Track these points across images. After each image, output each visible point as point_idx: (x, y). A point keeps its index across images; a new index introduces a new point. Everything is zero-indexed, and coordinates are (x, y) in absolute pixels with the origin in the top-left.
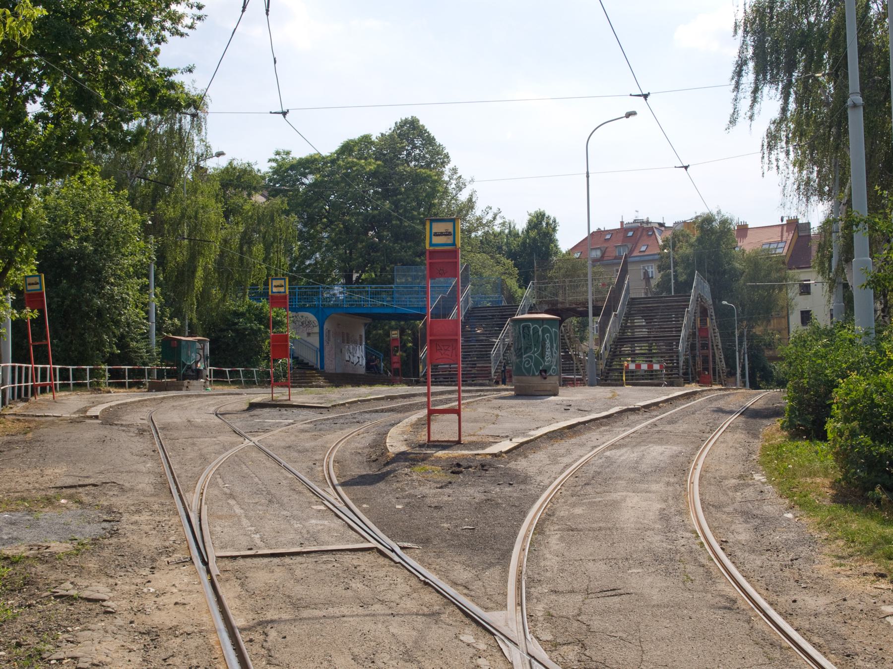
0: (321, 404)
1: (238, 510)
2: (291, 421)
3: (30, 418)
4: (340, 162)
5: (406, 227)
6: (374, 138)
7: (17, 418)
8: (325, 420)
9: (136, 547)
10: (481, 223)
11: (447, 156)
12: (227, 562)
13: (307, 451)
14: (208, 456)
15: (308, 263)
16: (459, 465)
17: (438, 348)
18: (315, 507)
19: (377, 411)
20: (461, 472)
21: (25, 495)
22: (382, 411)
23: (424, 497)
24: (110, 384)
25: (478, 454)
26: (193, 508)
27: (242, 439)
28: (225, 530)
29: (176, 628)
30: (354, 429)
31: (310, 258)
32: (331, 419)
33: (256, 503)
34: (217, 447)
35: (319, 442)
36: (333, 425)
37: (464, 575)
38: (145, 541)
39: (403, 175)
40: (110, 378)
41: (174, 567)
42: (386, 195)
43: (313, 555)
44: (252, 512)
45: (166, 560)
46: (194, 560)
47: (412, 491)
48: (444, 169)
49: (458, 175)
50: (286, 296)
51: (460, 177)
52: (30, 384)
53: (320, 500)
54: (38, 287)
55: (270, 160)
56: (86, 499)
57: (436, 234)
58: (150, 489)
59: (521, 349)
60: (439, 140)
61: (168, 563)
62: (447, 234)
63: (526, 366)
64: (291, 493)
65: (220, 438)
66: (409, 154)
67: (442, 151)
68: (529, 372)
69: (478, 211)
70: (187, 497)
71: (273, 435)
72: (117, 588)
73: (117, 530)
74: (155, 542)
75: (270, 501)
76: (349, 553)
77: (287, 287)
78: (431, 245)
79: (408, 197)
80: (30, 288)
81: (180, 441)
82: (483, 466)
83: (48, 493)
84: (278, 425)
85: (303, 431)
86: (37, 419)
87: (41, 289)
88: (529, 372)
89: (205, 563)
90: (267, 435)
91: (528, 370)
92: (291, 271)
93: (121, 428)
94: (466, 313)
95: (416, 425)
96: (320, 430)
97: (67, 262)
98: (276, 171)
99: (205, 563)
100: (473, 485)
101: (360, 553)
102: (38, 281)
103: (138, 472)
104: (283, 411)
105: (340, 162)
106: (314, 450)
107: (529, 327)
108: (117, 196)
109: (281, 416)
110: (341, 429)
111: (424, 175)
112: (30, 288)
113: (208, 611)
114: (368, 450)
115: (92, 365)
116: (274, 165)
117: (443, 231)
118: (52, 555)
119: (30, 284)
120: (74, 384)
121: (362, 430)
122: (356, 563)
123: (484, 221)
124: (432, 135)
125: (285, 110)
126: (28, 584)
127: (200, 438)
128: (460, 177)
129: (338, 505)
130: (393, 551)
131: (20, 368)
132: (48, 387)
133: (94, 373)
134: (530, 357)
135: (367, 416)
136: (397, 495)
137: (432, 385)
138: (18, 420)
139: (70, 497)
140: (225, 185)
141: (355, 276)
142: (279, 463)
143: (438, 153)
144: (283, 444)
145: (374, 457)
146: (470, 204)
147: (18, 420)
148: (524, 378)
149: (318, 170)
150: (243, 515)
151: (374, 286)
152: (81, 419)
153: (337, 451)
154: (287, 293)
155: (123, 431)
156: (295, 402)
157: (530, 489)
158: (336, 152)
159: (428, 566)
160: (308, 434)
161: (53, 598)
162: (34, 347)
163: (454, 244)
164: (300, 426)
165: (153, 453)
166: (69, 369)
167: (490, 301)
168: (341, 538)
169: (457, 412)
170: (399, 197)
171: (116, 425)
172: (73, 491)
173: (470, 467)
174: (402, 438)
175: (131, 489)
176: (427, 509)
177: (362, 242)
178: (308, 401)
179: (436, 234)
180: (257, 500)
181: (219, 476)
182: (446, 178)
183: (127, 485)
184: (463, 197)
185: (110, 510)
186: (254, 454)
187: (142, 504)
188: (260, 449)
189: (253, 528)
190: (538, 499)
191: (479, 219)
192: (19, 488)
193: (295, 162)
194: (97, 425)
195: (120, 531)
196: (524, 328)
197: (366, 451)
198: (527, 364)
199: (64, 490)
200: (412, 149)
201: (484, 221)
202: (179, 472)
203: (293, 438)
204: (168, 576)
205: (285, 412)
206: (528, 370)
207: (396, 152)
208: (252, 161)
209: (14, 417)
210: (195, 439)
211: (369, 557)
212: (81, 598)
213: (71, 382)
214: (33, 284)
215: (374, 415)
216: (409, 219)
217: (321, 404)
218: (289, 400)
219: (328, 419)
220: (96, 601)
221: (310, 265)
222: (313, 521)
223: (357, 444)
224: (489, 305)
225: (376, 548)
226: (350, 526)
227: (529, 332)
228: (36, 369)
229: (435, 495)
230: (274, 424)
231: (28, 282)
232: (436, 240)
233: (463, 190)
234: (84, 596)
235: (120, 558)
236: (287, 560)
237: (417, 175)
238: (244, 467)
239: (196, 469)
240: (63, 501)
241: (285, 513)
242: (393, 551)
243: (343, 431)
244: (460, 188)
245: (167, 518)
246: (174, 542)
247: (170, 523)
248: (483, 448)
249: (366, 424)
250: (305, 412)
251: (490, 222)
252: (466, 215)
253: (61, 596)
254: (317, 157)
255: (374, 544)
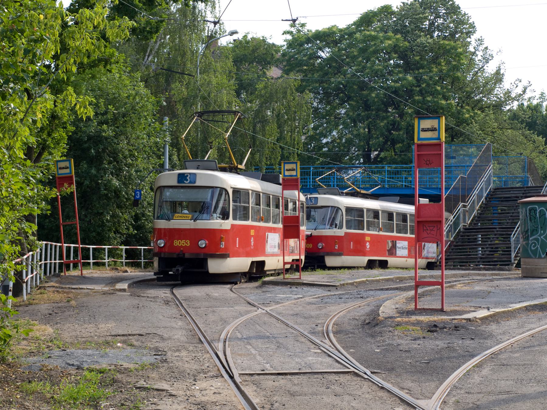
0: (330, 282)
1: (253, 352)
2: (301, 296)
3: (67, 290)
4: (358, 35)
5: (429, 101)
6: (395, 9)
7: (57, 289)
8: (331, 295)
9: (182, 369)
10: (509, 96)
11: (472, 26)
12: (246, 377)
13: (312, 317)
14: (227, 320)
15: (324, 141)
16: (435, 326)
17: (425, 228)
18: (313, 351)
19: (382, 290)
20: (436, 331)
21: (90, 339)
22: (387, 289)
23: (399, 345)
24: (127, 264)
25: (455, 319)
26: (220, 349)
27: (256, 309)
28: (244, 362)
29: (216, 402)
30: (359, 302)
31: (325, 136)
32: (337, 295)
33: (268, 348)
34: (234, 314)
35: (324, 311)
36: (338, 300)
37: (409, 384)
38: (187, 365)
39: (426, 46)
40: (126, 259)
41: (210, 379)
42: (408, 67)
43: (308, 375)
44: (264, 353)
45: (204, 376)
46: (224, 375)
47: (391, 342)
48: (469, 40)
49: (484, 46)
50: (297, 179)
51: (486, 48)
52: (58, 261)
53: (318, 347)
54: (67, 171)
55: (285, 33)
56: (135, 343)
57: (424, 130)
58: (183, 339)
59: (527, 231)
60: (464, 9)
61: (205, 377)
62: (433, 130)
63: (533, 248)
64: (295, 342)
65: (236, 308)
66: (432, 24)
67: (468, 20)
68: (535, 255)
69: (506, 84)
70: (215, 345)
71: (284, 306)
72: (174, 386)
73: (166, 359)
74: (195, 366)
75: (278, 347)
76: (333, 374)
77: (299, 170)
78: (419, 139)
79: (431, 71)
80: (61, 171)
81: (202, 309)
82: (456, 327)
83: (106, 339)
84: (288, 299)
85: (310, 303)
86: (73, 291)
87: (71, 173)
88: (535, 255)
89: (232, 377)
90: (277, 306)
91: (535, 252)
92: (308, 150)
93: (148, 299)
94: (488, 194)
95: (409, 300)
96: (326, 303)
97: (86, 145)
98: (291, 44)
99: (232, 377)
100: (441, 340)
101: (342, 375)
102: (68, 166)
103: (172, 328)
104: (294, 289)
105: (358, 35)
106: (318, 317)
107: (535, 210)
108: (131, 77)
109: (291, 292)
110: (345, 303)
111: (448, 47)
112: (61, 171)
113: (236, 396)
114: (364, 317)
115: (110, 245)
116: (289, 37)
117: (430, 127)
118: (125, 369)
119: (60, 168)
120: (94, 263)
121: (364, 303)
122: (337, 379)
123: (513, 95)
124: (457, 3)
125: (294, 18)
126: (116, 382)
127: (219, 307)
128: (486, 48)
129: (331, 349)
130: (365, 374)
131: (51, 245)
132: (72, 264)
133: (111, 253)
134: (537, 240)
135: (372, 293)
136: (379, 345)
137: (446, 269)
138: (58, 291)
139: (124, 342)
140: (238, 61)
141: (374, 154)
142: (287, 325)
143: (462, 22)
144: (291, 312)
145: (367, 321)
146: (498, 77)
147: (58, 291)
148: (530, 260)
149: (336, 43)
150: (257, 354)
151: (394, 166)
152: (112, 291)
153: (338, 318)
154: (299, 176)
155: (151, 301)
156: (306, 280)
157: (487, 343)
158: (354, 24)
159: (388, 381)
160: (314, 305)
161: (134, 389)
162: (64, 226)
163: (439, 139)
164: (307, 299)
165: (180, 317)
166: (89, 248)
167: (520, 182)
168: (331, 366)
169: (441, 284)
170: (421, 71)
171: (142, 296)
172: (125, 338)
173: (446, 328)
174: (394, 307)
175: (170, 338)
176: (398, 352)
177: (384, 118)
178: (318, 280)
179: (424, 130)
180: (268, 346)
181: (237, 331)
182: (471, 49)
183: (165, 336)
184: (490, 69)
185: (157, 349)
186: (266, 319)
187: (180, 347)
188: (271, 315)
189: (265, 361)
190: (490, 349)
191: (508, 92)
192: (84, 335)
193: (310, 35)
194: (128, 297)
195: (168, 360)
196: (530, 210)
197: (363, 318)
198: (534, 247)
199: (118, 337)
200: (435, 18)
201: (513, 95)
202: (205, 329)
203: (300, 308)
204: (207, 383)
205: (296, 289)
206: (535, 252)
207: (417, 22)
208: (267, 35)
209: (54, 289)
210: (214, 308)
211: (348, 377)
212: (153, 389)
213: (91, 261)
214: (63, 168)
215: (379, 292)
216: (432, 94)
217: (330, 282)
218: (300, 278)
219: (335, 295)
220: (163, 390)
221: (327, 143)
222: (310, 358)
223: (355, 313)
224: (518, 185)
225: (353, 372)
226: (337, 361)
227: (536, 215)
228: (70, 247)
229: (407, 344)
230: (284, 298)
231: (59, 167)
232: (423, 135)
233: (490, 62)
234: (155, 388)
235: (172, 374)
236: (289, 377)
237: (440, 47)
238: (258, 327)
239: (219, 328)
240: (119, 344)
241: (289, 353)
242: (365, 374)
243: (346, 304)
244: (487, 60)
245: (200, 354)
246: (208, 367)
247: (203, 357)
248: (460, 315)
249: (368, 299)
250: (314, 289)
251: (520, 95)
252: (492, 89)
253: (139, 388)
254: (334, 29)
255: (353, 369)
